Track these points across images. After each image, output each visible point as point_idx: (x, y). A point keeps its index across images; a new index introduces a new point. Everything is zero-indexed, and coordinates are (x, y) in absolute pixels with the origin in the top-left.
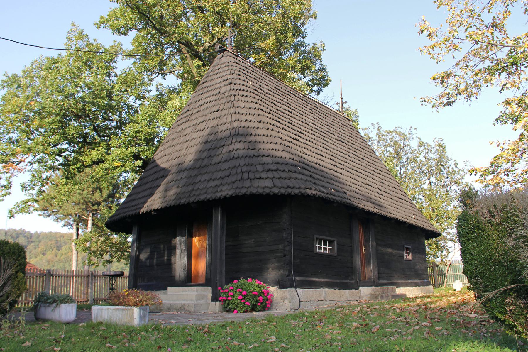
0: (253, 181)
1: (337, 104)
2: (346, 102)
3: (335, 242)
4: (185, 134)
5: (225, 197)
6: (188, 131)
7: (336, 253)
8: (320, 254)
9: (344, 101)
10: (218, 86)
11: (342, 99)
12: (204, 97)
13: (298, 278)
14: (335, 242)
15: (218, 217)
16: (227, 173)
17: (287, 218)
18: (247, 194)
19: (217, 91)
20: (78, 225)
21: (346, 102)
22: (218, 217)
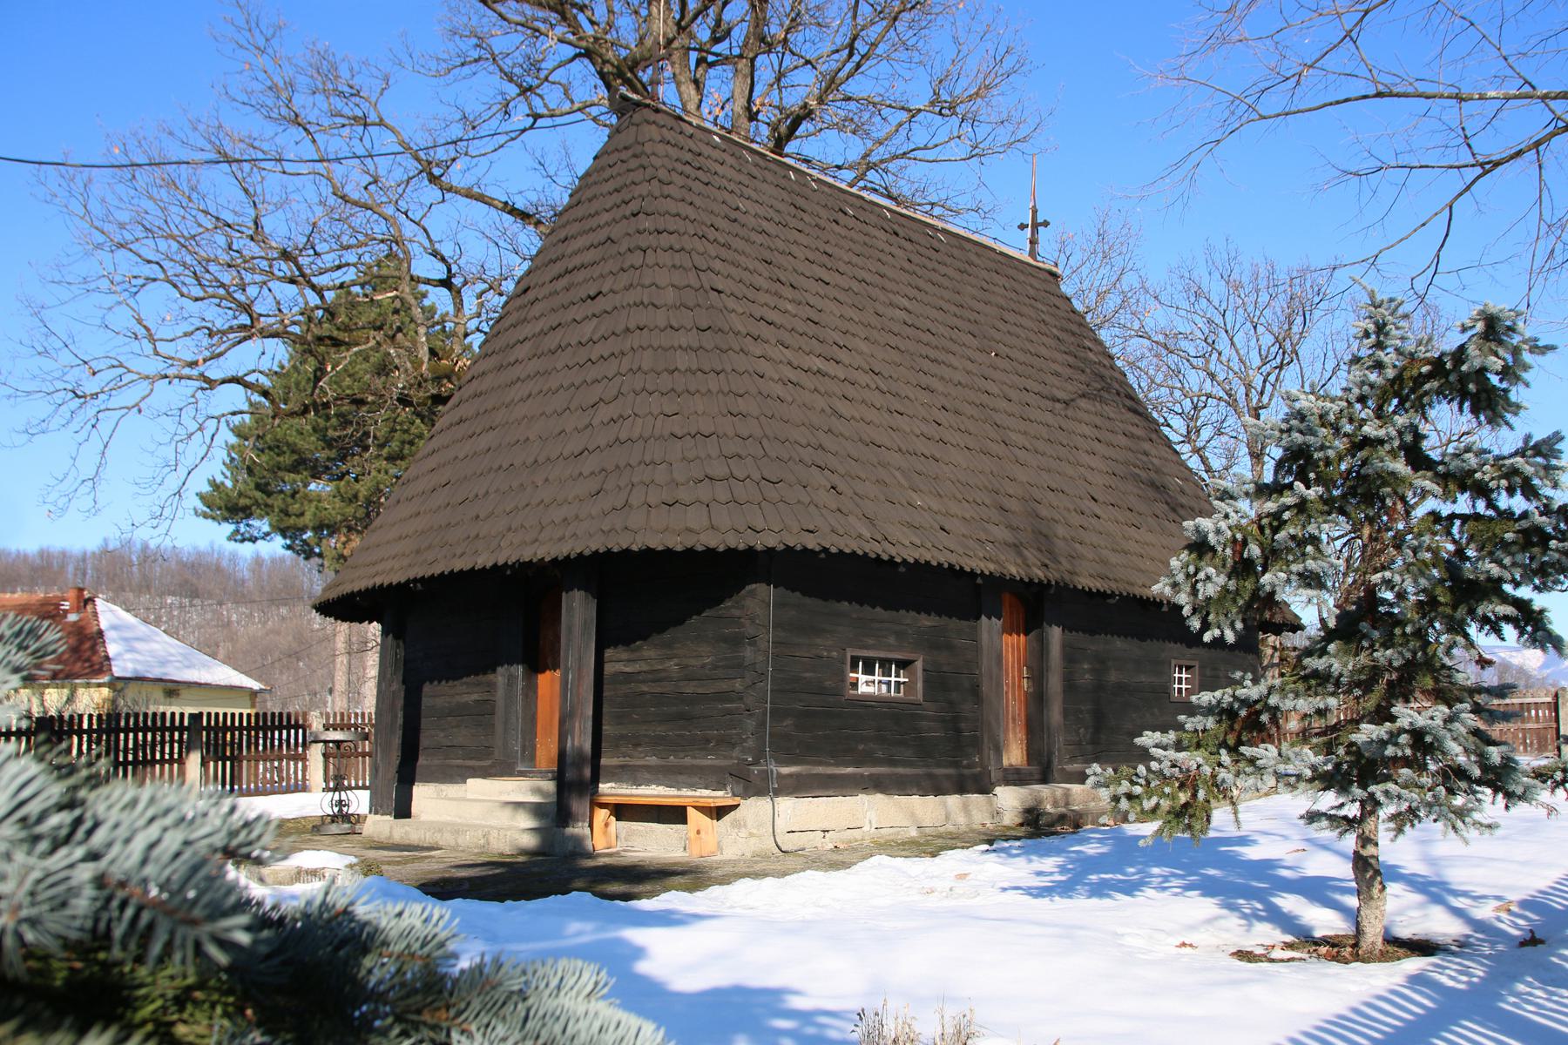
0: (653, 511)
1: (1022, 227)
2: (1046, 224)
3: (919, 665)
4: (512, 360)
5: (580, 554)
6: (521, 352)
7: (919, 695)
8: (866, 700)
9: (1040, 220)
10: (606, 217)
11: (1035, 212)
12: (569, 251)
13: (785, 770)
14: (919, 665)
15: (578, 612)
16: (593, 485)
17: (760, 601)
18: (635, 548)
19: (601, 235)
20: (265, 394)
21: (1046, 224)
22: (578, 612)
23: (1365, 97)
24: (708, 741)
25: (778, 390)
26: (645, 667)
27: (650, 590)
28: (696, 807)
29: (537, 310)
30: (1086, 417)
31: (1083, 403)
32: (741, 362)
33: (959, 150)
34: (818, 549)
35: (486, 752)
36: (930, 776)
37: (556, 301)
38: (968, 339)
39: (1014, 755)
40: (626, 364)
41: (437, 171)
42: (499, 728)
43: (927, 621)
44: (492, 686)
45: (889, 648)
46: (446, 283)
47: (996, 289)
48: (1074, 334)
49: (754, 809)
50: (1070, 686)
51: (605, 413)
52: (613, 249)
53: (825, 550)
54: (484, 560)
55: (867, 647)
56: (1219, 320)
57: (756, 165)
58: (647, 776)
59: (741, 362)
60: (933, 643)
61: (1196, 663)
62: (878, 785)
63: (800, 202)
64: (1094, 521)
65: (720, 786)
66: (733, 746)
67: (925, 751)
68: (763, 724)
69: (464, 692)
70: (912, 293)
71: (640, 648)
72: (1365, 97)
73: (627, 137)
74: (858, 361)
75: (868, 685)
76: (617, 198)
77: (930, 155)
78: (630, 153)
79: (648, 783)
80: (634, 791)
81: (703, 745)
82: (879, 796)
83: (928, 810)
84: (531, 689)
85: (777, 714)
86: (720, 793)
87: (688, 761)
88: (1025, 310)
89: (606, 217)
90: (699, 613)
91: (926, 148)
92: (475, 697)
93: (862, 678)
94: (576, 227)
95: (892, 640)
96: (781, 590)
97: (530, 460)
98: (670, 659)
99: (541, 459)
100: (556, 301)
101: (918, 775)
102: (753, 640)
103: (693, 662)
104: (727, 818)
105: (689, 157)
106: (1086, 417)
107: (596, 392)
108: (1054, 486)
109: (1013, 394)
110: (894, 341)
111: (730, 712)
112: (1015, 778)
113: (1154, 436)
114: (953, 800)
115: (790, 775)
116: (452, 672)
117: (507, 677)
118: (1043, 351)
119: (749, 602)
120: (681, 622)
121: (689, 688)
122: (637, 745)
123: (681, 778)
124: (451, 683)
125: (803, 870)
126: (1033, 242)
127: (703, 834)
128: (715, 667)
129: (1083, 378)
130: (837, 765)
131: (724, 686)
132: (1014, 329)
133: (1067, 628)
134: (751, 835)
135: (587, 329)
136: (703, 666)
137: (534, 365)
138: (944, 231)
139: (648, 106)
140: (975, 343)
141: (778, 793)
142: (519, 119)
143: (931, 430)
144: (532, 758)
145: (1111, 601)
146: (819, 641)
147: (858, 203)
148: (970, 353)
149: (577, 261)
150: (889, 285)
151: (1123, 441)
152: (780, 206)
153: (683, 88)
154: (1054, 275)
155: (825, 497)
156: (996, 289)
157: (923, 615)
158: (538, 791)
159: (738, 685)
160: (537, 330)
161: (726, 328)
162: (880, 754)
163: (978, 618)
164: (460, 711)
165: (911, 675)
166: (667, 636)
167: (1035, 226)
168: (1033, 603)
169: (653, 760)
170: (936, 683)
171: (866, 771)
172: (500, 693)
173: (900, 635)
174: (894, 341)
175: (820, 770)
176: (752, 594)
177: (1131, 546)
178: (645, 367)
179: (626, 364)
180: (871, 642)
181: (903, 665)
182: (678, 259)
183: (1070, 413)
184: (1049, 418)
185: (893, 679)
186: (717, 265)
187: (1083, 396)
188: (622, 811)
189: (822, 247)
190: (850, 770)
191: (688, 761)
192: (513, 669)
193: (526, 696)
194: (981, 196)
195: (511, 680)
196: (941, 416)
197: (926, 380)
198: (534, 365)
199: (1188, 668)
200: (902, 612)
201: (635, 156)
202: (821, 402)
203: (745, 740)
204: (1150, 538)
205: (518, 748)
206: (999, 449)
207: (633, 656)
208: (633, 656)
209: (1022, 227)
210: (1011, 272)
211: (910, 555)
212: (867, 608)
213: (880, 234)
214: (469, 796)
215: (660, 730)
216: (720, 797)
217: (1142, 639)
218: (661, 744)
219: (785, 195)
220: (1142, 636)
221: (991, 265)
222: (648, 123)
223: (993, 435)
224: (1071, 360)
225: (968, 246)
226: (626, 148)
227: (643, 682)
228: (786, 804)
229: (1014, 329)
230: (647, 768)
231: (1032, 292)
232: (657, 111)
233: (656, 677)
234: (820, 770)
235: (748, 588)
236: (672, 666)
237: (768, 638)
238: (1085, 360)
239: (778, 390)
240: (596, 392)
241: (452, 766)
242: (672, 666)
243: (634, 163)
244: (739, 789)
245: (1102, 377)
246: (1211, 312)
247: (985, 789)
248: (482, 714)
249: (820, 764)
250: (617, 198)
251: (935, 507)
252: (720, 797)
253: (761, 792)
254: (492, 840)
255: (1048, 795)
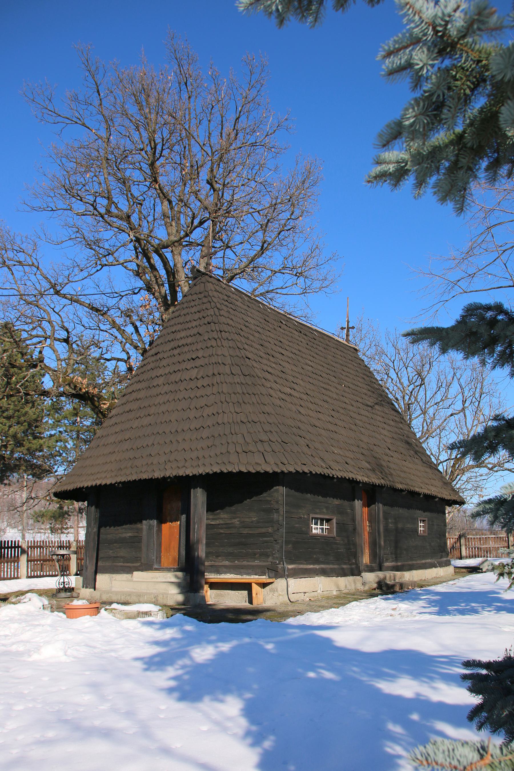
1: (342, 328)
2: (353, 328)
3: (334, 521)
7: (426, 534)
8: (316, 536)
10: (194, 324)
11: (348, 322)
13: (290, 567)
14: (334, 521)
15: (199, 497)
21: (353, 328)
22: (199, 497)
23: (510, 286)
24: (255, 554)
25: (278, 402)
26: (222, 522)
27: (229, 489)
28: (256, 583)
29: (164, 363)
30: (379, 413)
31: (377, 407)
32: (263, 390)
33: (297, 290)
34: (308, 472)
35: (137, 559)
36: (343, 569)
37: (175, 360)
38: (333, 379)
39: (366, 559)
40: (215, 390)
41: (58, 288)
42: (144, 548)
43: (337, 502)
44: (140, 530)
45: (323, 513)
46: (66, 341)
47: (338, 356)
48: (368, 376)
49: (280, 583)
50: (386, 530)
51: (208, 411)
52: (201, 338)
53: (311, 472)
54: (158, 475)
55: (316, 513)
56: (391, 364)
57: (249, 302)
58: (225, 570)
59: (263, 390)
60: (340, 511)
61: (426, 519)
62: (325, 573)
63: (267, 319)
64: (391, 458)
65: (263, 574)
66: (268, 556)
67: (338, 558)
68: (282, 547)
69: (125, 532)
70: (312, 358)
71: (219, 513)
72: (510, 286)
73: (197, 289)
74: (302, 390)
75: (316, 529)
76: (200, 315)
77: (284, 291)
78: (203, 295)
79: (225, 573)
80: (218, 576)
81: (253, 556)
82: (322, 577)
83: (346, 583)
84: (160, 531)
85: (287, 542)
86: (264, 577)
87: (245, 563)
88: (350, 366)
89: (194, 324)
90: (250, 498)
91: (282, 288)
92: (130, 534)
93: (314, 526)
94: (179, 327)
95: (325, 510)
96: (288, 489)
97: (173, 431)
98: (234, 518)
99: (179, 430)
100: (175, 360)
101: (335, 568)
102: (277, 511)
103: (247, 520)
104: (268, 588)
105: (226, 298)
106: (379, 413)
107: (202, 402)
108: (376, 444)
109: (354, 403)
110: (311, 380)
111: (266, 542)
112: (371, 570)
113: (402, 421)
114: (351, 578)
115: (292, 569)
116: (118, 522)
117: (147, 525)
118: (360, 385)
119: (275, 494)
120: (241, 502)
121: (245, 531)
122: (217, 556)
123: (242, 570)
124: (117, 528)
125: (331, 607)
126: (348, 335)
127: (258, 595)
128: (258, 522)
129: (374, 395)
130: (307, 564)
131: (263, 530)
132: (347, 374)
133: (384, 505)
134: (280, 595)
135: (194, 373)
136: (252, 522)
137: (166, 388)
138: (316, 330)
139: (207, 274)
140: (336, 380)
141: (289, 576)
142: (99, 267)
143: (330, 419)
144: (160, 562)
145: (404, 493)
146: (300, 511)
147: (286, 318)
148: (335, 385)
149: (183, 342)
150: (304, 356)
151: (392, 423)
152: (261, 320)
153: (176, 257)
154: (356, 350)
155: (306, 449)
156: (338, 356)
157: (335, 500)
158: (176, 577)
159: (270, 530)
160: (167, 372)
161: (255, 375)
162: (321, 559)
163: (354, 500)
164: (122, 541)
165: (331, 525)
166: (233, 508)
167: (348, 328)
168: (371, 494)
169: (227, 563)
170: (341, 527)
171: (317, 567)
172: (145, 533)
173: (327, 508)
174: (311, 380)
175: (302, 566)
176: (277, 491)
177: (405, 469)
178: (225, 391)
179: (215, 390)
180: (318, 511)
181: (328, 521)
182: (231, 344)
183: (374, 411)
184: (367, 414)
185: (324, 527)
186: (246, 347)
187: (376, 404)
188: (214, 586)
189: (279, 339)
190: (312, 566)
191: (245, 563)
192: (151, 522)
193: (158, 534)
194: (325, 316)
195: (150, 528)
196: (333, 413)
197: (326, 398)
198: (166, 388)
199: (423, 521)
200: (328, 498)
201: (205, 297)
202: (294, 408)
203: (274, 554)
204: (410, 465)
205: (154, 558)
206: (353, 427)
207: (215, 517)
208: (215, 517)
209: (342, 328)
210: (342, 349)
211: (340, 474)
212: (316, 496)
213: (295, 332)
214: (134, 579)
215: (230, 550)
216: (264, 579)
217: (408, 509)
218: (229, 556)
219: (261, 315)
220: (409, 507)
221: (334, 346)
222: (208, 282)
223: (351, 422)
224: (369, 388)
225: (325, 337)
226: (200, 293)
227: (222, 528)
228: (292, 581)
229: (347, 374)
230: (225, 567)
231: (350, 358)
232: (211, 277)
233: (228, 526)
234: (302, 566)
235: (275, 488)
236: (236, 522)
237: (283, 509)
238: (374, 388)
239: (278, 402)
240: (202, 402)
241: (118, 566)
242: (236, 522)
243: (205, 300)
244: (272, 574)
245: (381, 395)
246: (387, 361)
247: (359, 574)
248: (135, 542)
249: (302, 564)
250: (200, 315)
251: (341, 453)
252: (264, 579)
253: (282, 576)
254: (159, 599)
255: (390, 576)
